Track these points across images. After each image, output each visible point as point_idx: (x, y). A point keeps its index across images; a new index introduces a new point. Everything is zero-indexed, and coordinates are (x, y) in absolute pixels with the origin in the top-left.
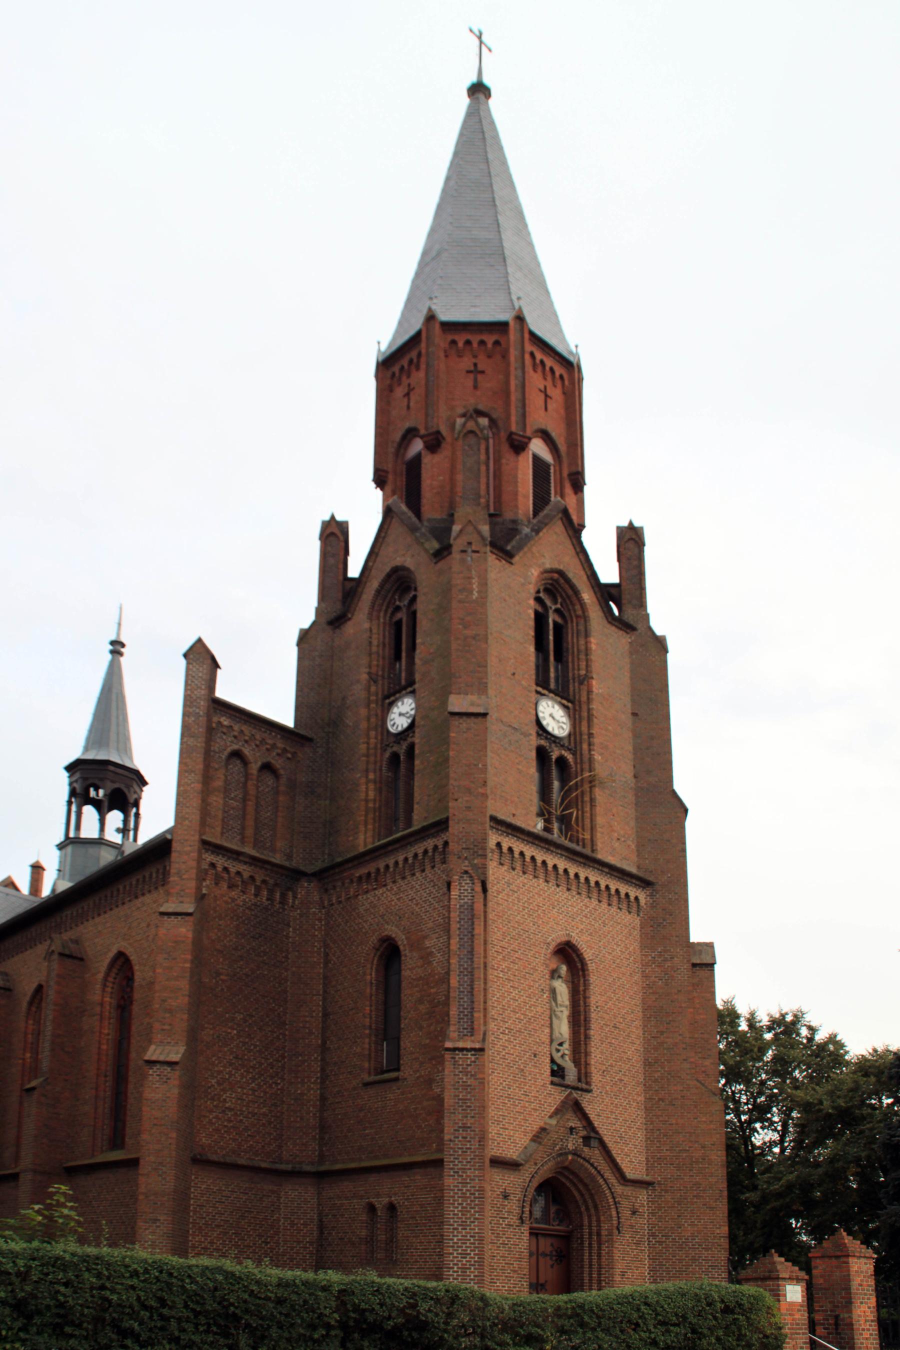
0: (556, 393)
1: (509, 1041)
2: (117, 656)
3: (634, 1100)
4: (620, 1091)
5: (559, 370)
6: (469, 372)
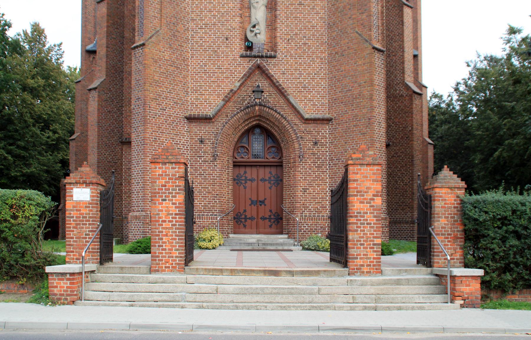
1: (206, 33)
4: (304, 52)
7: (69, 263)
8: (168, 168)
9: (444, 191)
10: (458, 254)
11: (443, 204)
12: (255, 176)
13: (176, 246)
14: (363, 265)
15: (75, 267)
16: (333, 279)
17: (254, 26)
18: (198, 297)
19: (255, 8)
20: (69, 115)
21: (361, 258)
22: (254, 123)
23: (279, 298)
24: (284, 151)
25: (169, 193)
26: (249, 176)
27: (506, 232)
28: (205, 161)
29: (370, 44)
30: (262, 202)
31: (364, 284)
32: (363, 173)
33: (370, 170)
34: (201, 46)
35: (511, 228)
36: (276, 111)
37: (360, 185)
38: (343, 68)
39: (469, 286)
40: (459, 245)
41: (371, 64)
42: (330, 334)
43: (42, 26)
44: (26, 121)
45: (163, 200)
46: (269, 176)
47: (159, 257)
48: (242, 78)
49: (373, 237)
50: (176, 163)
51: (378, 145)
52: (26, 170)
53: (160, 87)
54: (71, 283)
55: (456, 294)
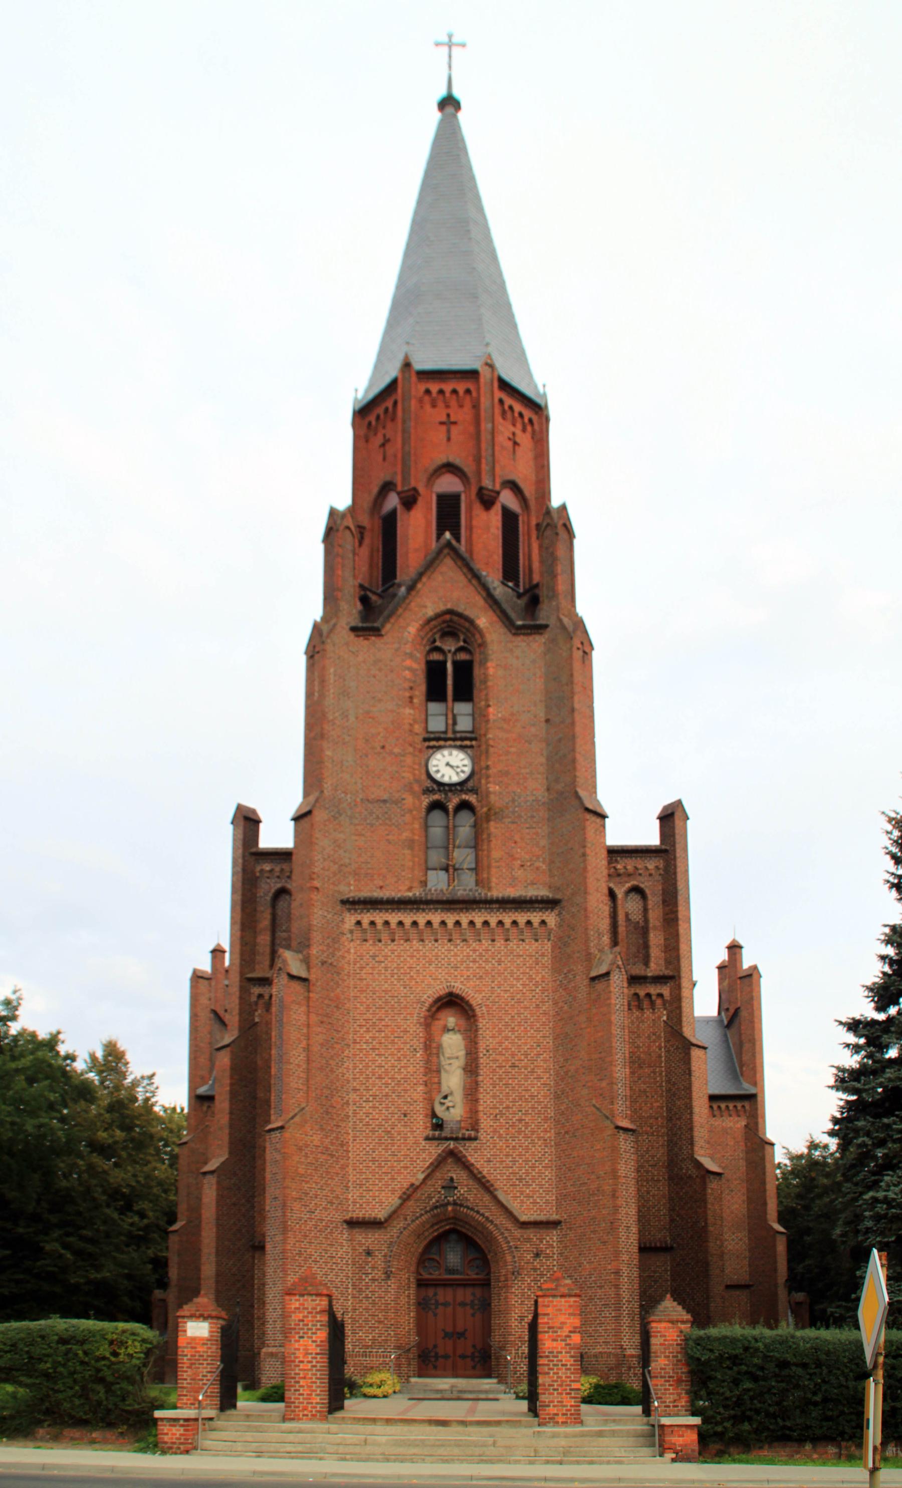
0: (525, 440)
1: (374, 1107)
2: (450, 110)
3: (539, 1138)
4: (519, 1132)
5: (528, 414)
6: (442, 423)
7: (181, 1408)
8: (307, 1300)
9: (663, 1325)
10: (683, 1400)
11: (661, 1340)
12: (449, 1298)
13: (315, 1391)
14: (557, 1414)
15: (191, 1413)
16: (518, 1430)
17: (445, 1097)
18: (341, 1449)
19: (446, 1071)
20: (167, 1187)
21: (554, 1406)
22: (447, 1227)
23: (441, 1451)
24: (492, 1265)
25: (309, 1329)
26: (441, 1299)
27: (739, 1373)
28: (373, 1280)
29: (612, 1122)
30: (462, 1335)
31: (555, 1436)
32: (555, 1306)
33: (566, 1302)
34: (368, 1124)
35: (744, 1368)
36: (478, 1212)
37: (552, 1319)
38: (575, 1154)
39: (683, 1436)
40: (683, 1389)
41: (615, 1149)
42: (485, 1482)
43: (122, 1046)
44: (94, 1199)
45: (301, 1337)
46: (472, 1298)
47: (294, 1403)
48: (428, 1167)
49: (571, 1381)
50: (317, 1295)
51: (625, 1257)
52: (94, 1275)
53: (307, 1182)
54: (185, 1430)
55: (666, 1446)
